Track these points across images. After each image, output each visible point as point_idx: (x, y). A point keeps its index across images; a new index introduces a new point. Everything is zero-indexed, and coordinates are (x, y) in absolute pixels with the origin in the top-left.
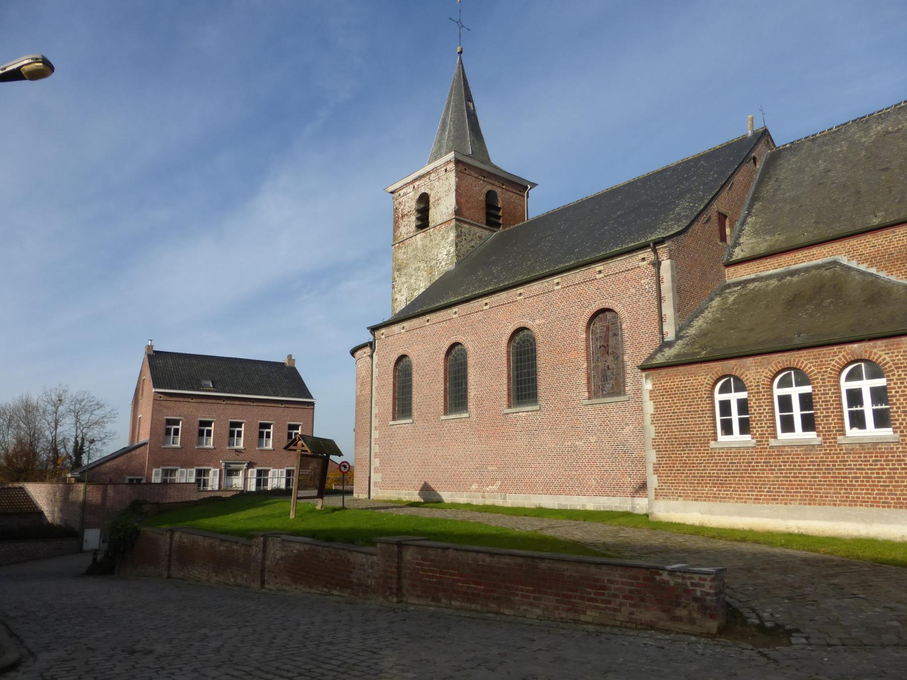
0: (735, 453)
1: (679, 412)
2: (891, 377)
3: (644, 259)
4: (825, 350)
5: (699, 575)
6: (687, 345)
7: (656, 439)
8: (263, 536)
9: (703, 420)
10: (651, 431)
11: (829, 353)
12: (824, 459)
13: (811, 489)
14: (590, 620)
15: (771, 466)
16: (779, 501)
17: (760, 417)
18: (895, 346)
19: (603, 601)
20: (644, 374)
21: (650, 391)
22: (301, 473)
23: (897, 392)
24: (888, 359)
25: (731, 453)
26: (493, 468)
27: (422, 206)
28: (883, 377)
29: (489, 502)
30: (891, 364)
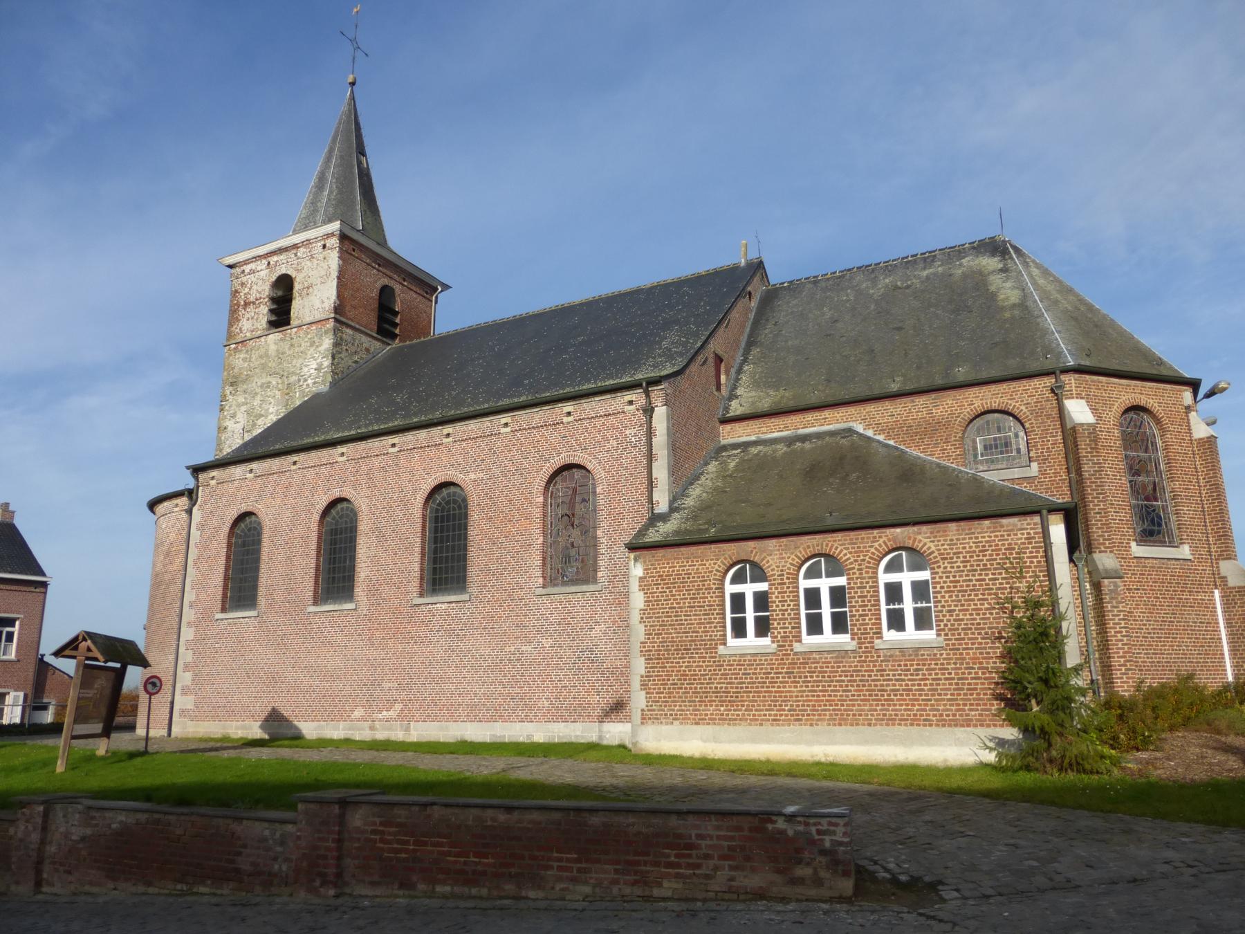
0: (750, 661)
1: (679, 608)
2: (937, 570)
3: (631, 403)
4: (863, 534)
5: (828, 819)
6: (687, 519)
7: (646, 643)
8: (43, 803)
9: (711, 619)
10: (639, 632)
11: (868, 538)
12: (859, 668)
13: (842, 705)
14: (669, 894)
15: (795, 677)
16: (804, 722)
17: (783, 615)
18: (941, 533)
19: (689, 866)
20: (632, 555)
21: (640, 578)
22: (81, 695)
23: (942, 588)
24: (933, 548)
25: (745, 661)
26: (391, 685)
27: (280, 293)
28: (766, 581)
29: (381, 735)
30: (936, 554)
